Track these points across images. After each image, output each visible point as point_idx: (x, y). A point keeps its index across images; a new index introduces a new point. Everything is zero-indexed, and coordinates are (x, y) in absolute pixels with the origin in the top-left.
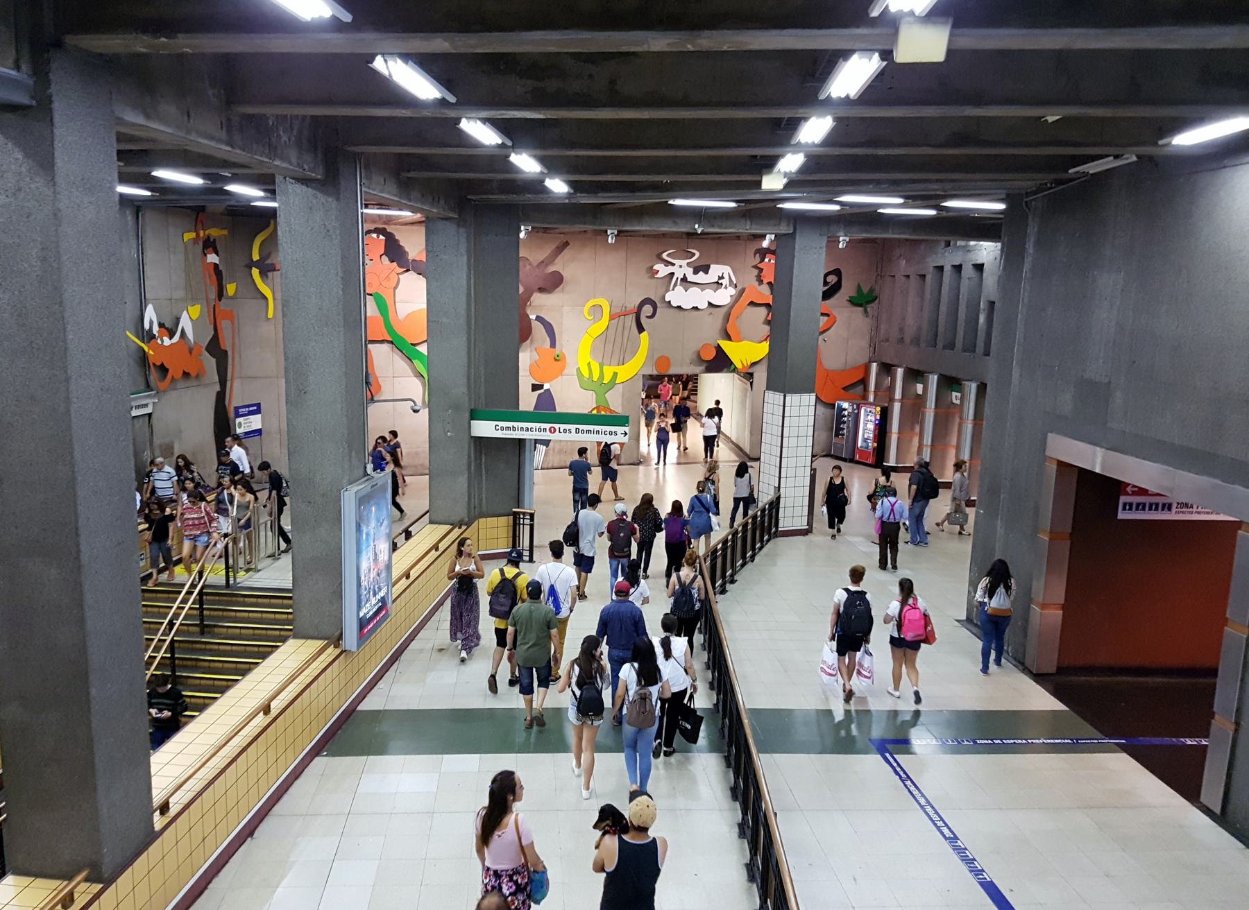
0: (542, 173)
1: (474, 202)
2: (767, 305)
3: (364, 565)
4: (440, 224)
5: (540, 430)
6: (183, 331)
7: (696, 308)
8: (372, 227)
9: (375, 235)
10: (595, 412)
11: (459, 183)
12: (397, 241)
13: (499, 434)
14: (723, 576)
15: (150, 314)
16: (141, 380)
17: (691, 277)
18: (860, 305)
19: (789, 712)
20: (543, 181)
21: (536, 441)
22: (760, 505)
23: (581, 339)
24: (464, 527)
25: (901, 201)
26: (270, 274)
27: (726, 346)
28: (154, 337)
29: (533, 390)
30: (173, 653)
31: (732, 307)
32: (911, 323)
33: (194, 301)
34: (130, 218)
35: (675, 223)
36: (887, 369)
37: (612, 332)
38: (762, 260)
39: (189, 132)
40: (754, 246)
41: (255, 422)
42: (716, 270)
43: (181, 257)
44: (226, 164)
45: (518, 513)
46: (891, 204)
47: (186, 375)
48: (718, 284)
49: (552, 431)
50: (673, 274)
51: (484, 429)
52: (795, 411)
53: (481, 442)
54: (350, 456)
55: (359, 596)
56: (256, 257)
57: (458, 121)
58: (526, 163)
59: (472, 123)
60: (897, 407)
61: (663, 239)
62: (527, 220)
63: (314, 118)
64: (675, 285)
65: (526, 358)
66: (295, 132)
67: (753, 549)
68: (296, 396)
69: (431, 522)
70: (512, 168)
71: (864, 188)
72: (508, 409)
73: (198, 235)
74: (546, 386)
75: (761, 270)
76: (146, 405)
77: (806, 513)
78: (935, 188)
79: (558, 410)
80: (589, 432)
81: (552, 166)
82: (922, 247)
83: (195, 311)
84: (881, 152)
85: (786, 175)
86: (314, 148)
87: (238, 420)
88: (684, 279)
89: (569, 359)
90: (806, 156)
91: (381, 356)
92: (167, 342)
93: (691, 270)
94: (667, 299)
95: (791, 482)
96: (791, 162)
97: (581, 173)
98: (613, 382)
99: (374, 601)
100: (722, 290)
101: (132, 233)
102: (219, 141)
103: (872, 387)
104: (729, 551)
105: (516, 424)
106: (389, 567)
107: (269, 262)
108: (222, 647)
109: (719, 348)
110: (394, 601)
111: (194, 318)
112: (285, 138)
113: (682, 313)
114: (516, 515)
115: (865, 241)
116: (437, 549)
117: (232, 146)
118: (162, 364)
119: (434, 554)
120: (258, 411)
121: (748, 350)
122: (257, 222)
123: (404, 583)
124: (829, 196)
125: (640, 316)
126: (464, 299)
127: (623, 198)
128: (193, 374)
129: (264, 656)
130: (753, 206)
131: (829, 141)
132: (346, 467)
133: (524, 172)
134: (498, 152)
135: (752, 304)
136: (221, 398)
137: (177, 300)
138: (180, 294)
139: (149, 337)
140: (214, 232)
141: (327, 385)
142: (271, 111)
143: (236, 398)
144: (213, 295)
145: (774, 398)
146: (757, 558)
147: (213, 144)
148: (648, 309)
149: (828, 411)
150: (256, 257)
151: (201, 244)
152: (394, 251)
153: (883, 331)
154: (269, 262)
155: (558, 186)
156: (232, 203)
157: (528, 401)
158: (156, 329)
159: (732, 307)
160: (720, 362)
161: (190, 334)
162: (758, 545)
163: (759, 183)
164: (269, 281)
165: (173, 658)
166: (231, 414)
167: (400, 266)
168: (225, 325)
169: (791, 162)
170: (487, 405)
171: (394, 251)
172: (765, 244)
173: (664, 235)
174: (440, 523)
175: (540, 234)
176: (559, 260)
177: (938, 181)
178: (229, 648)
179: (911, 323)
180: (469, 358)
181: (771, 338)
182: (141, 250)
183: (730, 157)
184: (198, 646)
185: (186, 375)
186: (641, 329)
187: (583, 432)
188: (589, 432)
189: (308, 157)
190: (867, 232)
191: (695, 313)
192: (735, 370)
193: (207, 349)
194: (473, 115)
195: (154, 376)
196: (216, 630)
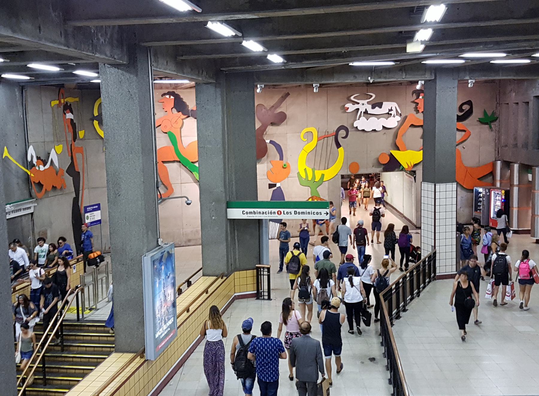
0: (264, 51)
1: (225, 71)
2: (422, 126)
3: (158, 304)
4: (205, 87)
5: (271, 213)
6: (52, 161)
7: (374, 131)
8: (166, 91)
9: (168, 96)
10: (310, 200)
11: (215, 60)
12: (182, 99)
13: (245, 217)
14: (398, 307)
15: (31, 151)
16: (26, 192)
17: (370, 111)
18: (487, 124)
20: (266, 56)
21: (270, 220)
22: (422, 258)
23: (299, 155)
24: (225, 278)
25: (504, 55)
27: (395, 153)
28: (34, 165)
29: (269, 188)
30: (44, 365)
31: (399, 129)
32: (521, 133)
33: (59, 142)
34: (18, 93)
35: (355, 77)
36: (507, 165)
37: (319, 148)
38: (418, 97)
39: (40, 39)
40: (410, 90)
41: (97, 215)
42: (387, 106)
43: (51, 116)
44: (71, 58)
45: (260, 268)
46: (498, 57)
48: (389, 114)
50: (358, 109)
51: (236, 213)
52: (443, 195)
53: (234, 222)
54: (148, 234)
55: (155, 324)
56: (96, 114)
57: (206, 23)
58: (253, 46)
59: (215, 24)
60: (516, 190)
62: (260, 81)
63: (120, 27)
64: (360, 116)
65: (262, 168)
66: (108, 36)
67: (418, 288)
68: (114, 197)
69: (203, 275)
70: (244, 50)
71: (477, 48)
72: (249, 198)
73: (60, 102)
74: (278, 185)
75: (417, 104)
76: (30, 208)
78: (525, 46)
79: (286, 200)
80: (303, 213)
81: (270, 47)
82: (526, 83)
83: (60, 148)
84: (482, 24)
85: (422, 43)
86: (120, 43)
87: (86, 215)
88: (366, 112)
89: (292, 167)
90: (434, 30)
91: (174, 171)
92: (42, 168)
93: (370, 106)
95: (443, 242)
96: (424, 35)
97: (290, 50)
99: (165, 327)
100: (391, 118)
101: (19, 103)
102: (60, 44)
103: (498, 177)
104: (401, 290)
106: (174, 305)
108: (75, 360)
109: (391, 155)
110: (178, 328)
111: (59, 153)
112: (102, 40)
113: (365, 134)
114: (258, 269)
115: (486, 82)
116: (207, 293)
117: (68, 47)
118: (39, 182)
119: (205, 296)
120: (99, 209)
121: (410, 157)
122: (91, 92)
123: (186, 314)
124: (456, 54)
125: (338, 137)
126: (221, 132)
127: (318, 64)
129: (96, 364)
130: (405, 63)
131: (445, 19)
132: (145, 241)
133: (254, 52)
134: (233, 40)
135: (412, 126)
136: (76, 201)
138: (50, 138)
139: (31, 165)
140: (70, 100)
141: (133, 189)
142: (92, 24)
143: (86, 201)
144: (70, 138)
145: (428, 187)
146: (422, 294)
147: (55, 45)
148: (342, 133)
149: (469, 194)
151: (62, 107)
152: (180, 105)
153: (503, 141)
155: (276, 59)
156: (80, 81)
157: (264, 194)
158: (35, 161)
159: (399, 129)
160: (393, 165)
161: (56, 163)
162: (422, 286)
163: (405, 49)
165: (44, 367)
166: (83, 211)
167: (184, 114)
168: (78, 156)
169: (424, 35)
170: (237, 198)
171: (180, 105)
172: (418, 87)
173: (351, 85)
174: (209, 276)
175: (271, 89)
176: (284, 104)
177: (525, 40)
178: (79, 360)
179: (521, 133)
180: (225, 169)
181: (424, 149)
182: (25, 113)
183: (384, 34)
184: (60, 359)
185: (54, 188)
186: (338, 145)
187: (299, 213)
188: (303, 213)
189: (117, 51)
190: (485, 76)
191: (374, 134)
192: (403, 169)
194: (214, 19)
195: (34, 190)
196: (71, 348)
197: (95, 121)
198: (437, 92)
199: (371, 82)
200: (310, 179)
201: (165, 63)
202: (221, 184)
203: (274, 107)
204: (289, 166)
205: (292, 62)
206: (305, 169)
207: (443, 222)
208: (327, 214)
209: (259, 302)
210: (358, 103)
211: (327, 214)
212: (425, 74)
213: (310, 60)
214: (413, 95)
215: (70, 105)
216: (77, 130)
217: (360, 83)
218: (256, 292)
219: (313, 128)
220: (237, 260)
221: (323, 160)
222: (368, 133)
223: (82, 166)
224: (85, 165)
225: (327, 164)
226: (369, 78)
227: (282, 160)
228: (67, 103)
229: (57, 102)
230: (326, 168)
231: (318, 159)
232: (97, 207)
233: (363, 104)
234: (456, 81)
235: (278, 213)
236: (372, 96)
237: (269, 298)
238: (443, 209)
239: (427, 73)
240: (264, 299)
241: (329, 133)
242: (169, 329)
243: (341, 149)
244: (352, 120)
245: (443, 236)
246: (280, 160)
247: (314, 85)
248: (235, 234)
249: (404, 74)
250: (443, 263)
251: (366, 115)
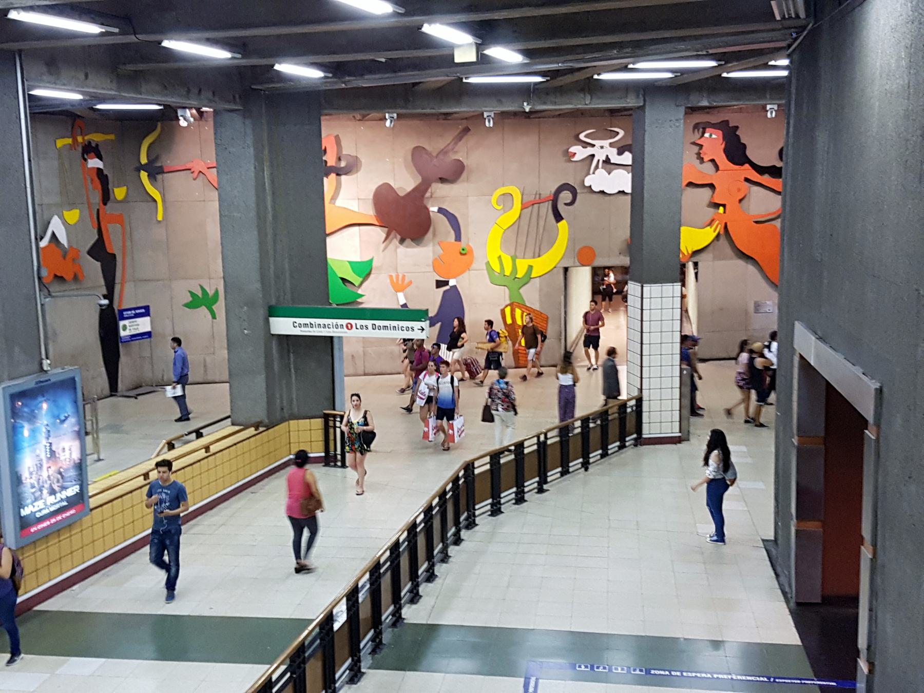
4: (227, 117)
17: (615, 159)
19: (675, 640)
26: (159, 177)
33: (72, 206)
35: (500, 101)
37: (525, 222)
41: (143, 325)
43: (56, 163)
49: (349, 327)
50: (593, 156)
51: (283, 326)
56: (144, 160)
61: (579, 117)
64: (597, 167)
73: (75, 140)
74: (452, 282)
87: (122, 323)
88: (607, 161)
89: (477, 253)
93: (615, 151)
94: (587, 184)
95: (655, 383)
98: (528, 278)
105: (313, 321)
113: (608, 198)
114: (326, 417)
125: (559, 202)
128: (68, 276)
135: (690, 184)
137: (49, 205)
144: (96, 197)
148: (566, 196)
150: (144, 160)
151: (80, 149)
161: (63, 239)
186: (558, 217)
188: (385, 327)
191: (600, 195)
197: (142, 172)
199: (527, 110)
200: (507, 273)
201: (82, 77)
202: (255, 276)
203: (444, 152)
204: (471, 251)
205: (349, 76)
206: (500, 257)
207: (655, 349)
208: (423, 329)
209: (331, 470)
210: (593, 146)
211: (423, 329)
213: (375, 73)
215: (97, 145)
216: (110, 187)
217: (597, 110)
218: (323, 454)
219: (515, 188)
221: (531, 242)
222: (612, 197)
224: (128, 243)
225: (537, 249)
227: (460, 240)
228: (90, 143)
230: (537, 255)
231: (522, 239)
232: (143, 311)
233: (602, 147)
236: (618, 133)
237: (344, 466)
238: (656, 326)
240: (335, 466)
241: (542, 197)
242: (65, 503)
243: (563, 224)
244: (584, 174)
245: (655, 372)
249: (588, 97)
251: (609, 166)
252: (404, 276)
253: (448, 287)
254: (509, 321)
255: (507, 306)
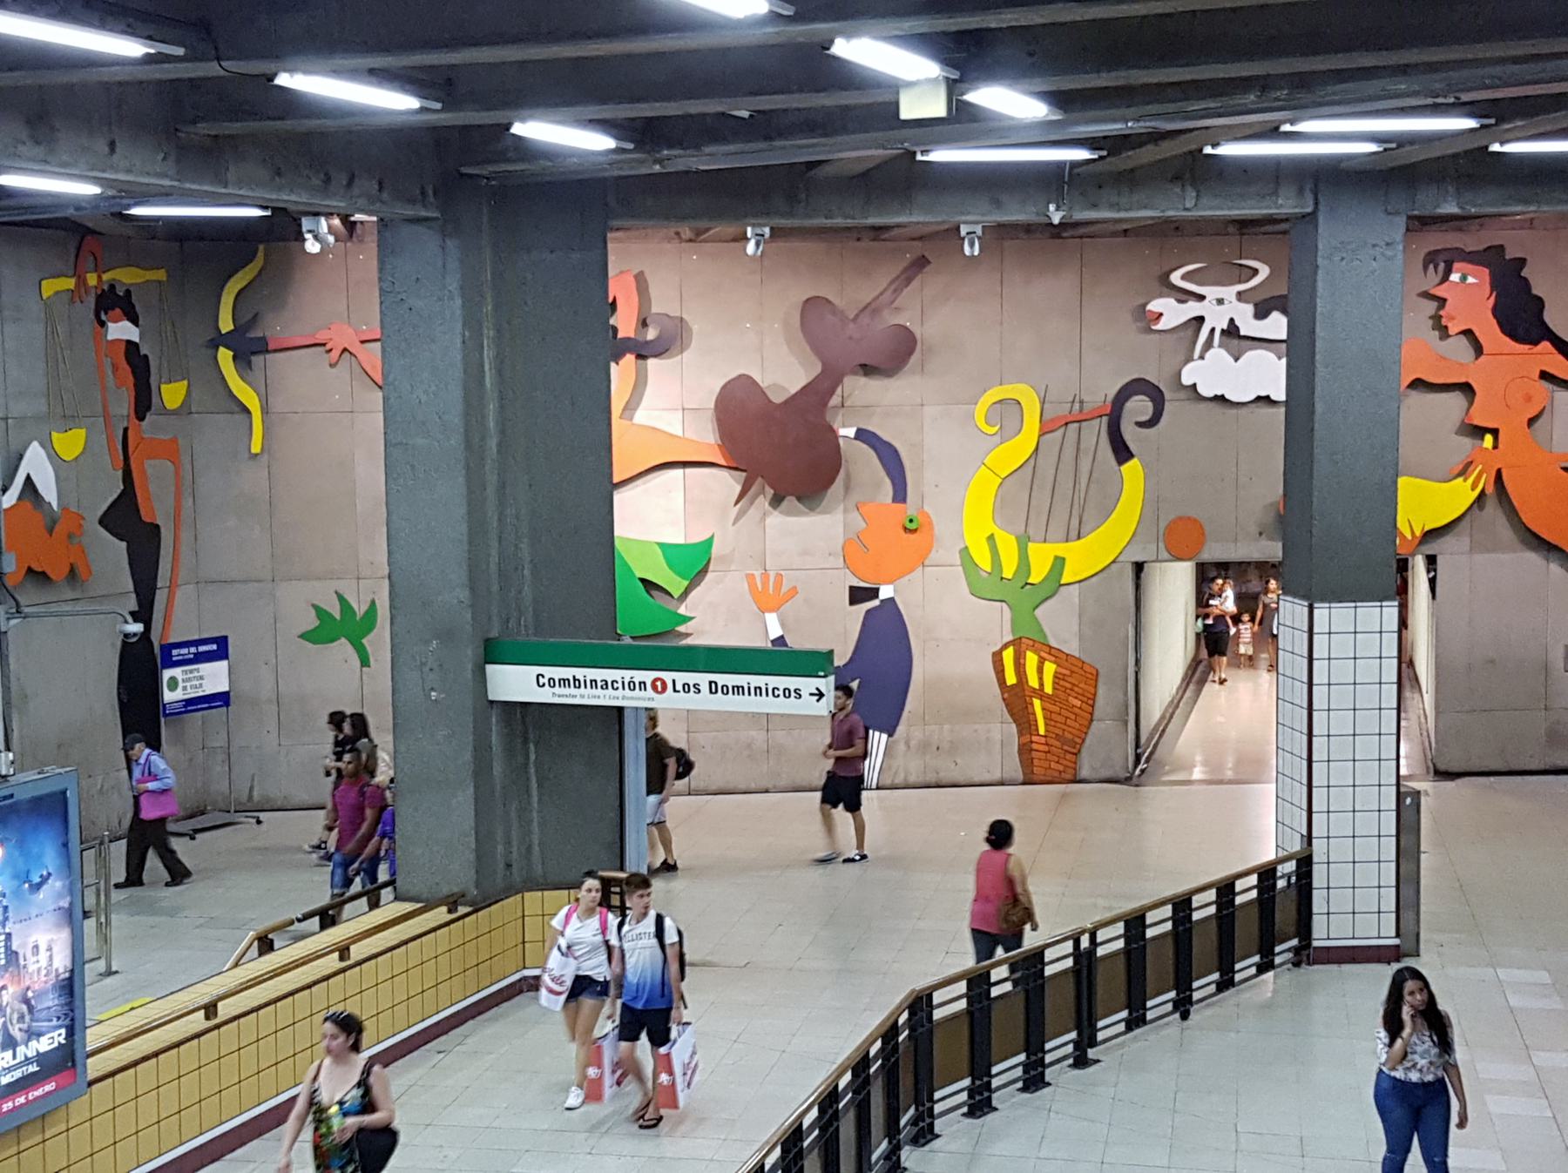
4: (407, 231)
5: (632, 685)
13: (546, 696)
17: (1249, 326)
29: (853, 602)
33: (68, 421)
38: (1445, 278)
41: (214, 677)
43: (39, 329)
47: (37, 576)
49: (659, 687)
51: (515, 683)
53: (523, 718)
56: (226, 325)
61: (1172, 236)
64: (1209, 344)
73: (82, 282)
74: (886, 592)
75: (1442, 302)
77: (1318, 898)
80: (738, 689)
87: (167, 674)
88: (1232, 331)
93: (1249, 309)
95: (1341, 824)
98: (1055, 583)
105: (580, 673)
107: (256, 333)
125: (1125, 419)
128: (58, 572)
143: (182, 618)
144: (123, 404)
148: (1139, 406)
150: (226, 325)
151: (91, 301)
154: (256, 333)
161: (49, 491)
164: (258, 372)
186: (1122, 453)
187: (725, 690)
188: (738, 689)
193: (101, 522)
197: (222, 350)
198: (1320, 260)
199: (1056, 221)
200: (1008, 573)
202: (458, 574)
203: (871, 309)
205: (670, 147)
206: (991, 538)
208: (821, 695)
210: (1201, 298)
211: (821, 695)
212: (1275, 193)
214: (1425, 268)
215: (128, 292)
220: (536, 848)
222: (1243, 411)
223: (171, 502)
225: (1075, 522)
226: (1052, 207)
227: (904, 500)
228: (112, 287)
229: (70, 283)
230: (1074, 534)
231: (1042, 498)
234: (1401, 222)
235: (654, 688)
236: (1255, 272)
239: (1283, 191)
241: (1087, 407)
242: (33, 1068)
243: (1132, 469)
246: (895, 500)
247: (964, 230)
248: (527, 758)
250: (1341, 900)
252: (779, 577)
253: (876, 603)
254: (1011, 679)
255: (1005, 646)
